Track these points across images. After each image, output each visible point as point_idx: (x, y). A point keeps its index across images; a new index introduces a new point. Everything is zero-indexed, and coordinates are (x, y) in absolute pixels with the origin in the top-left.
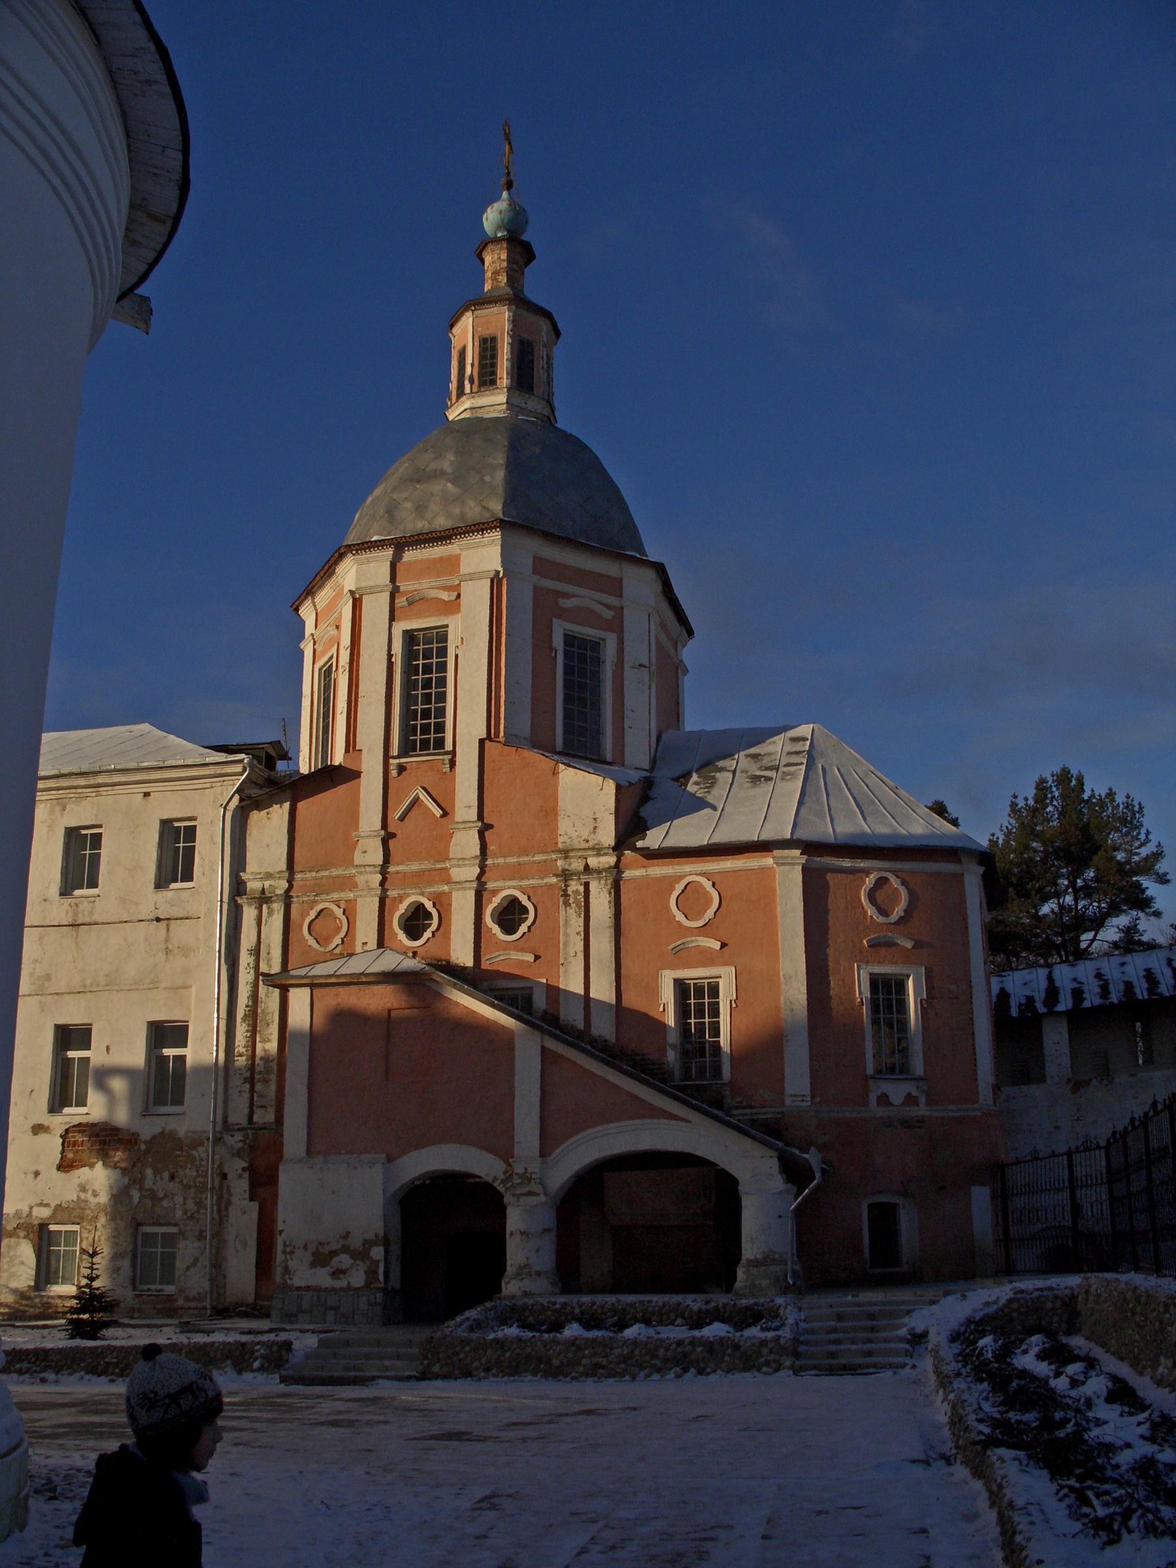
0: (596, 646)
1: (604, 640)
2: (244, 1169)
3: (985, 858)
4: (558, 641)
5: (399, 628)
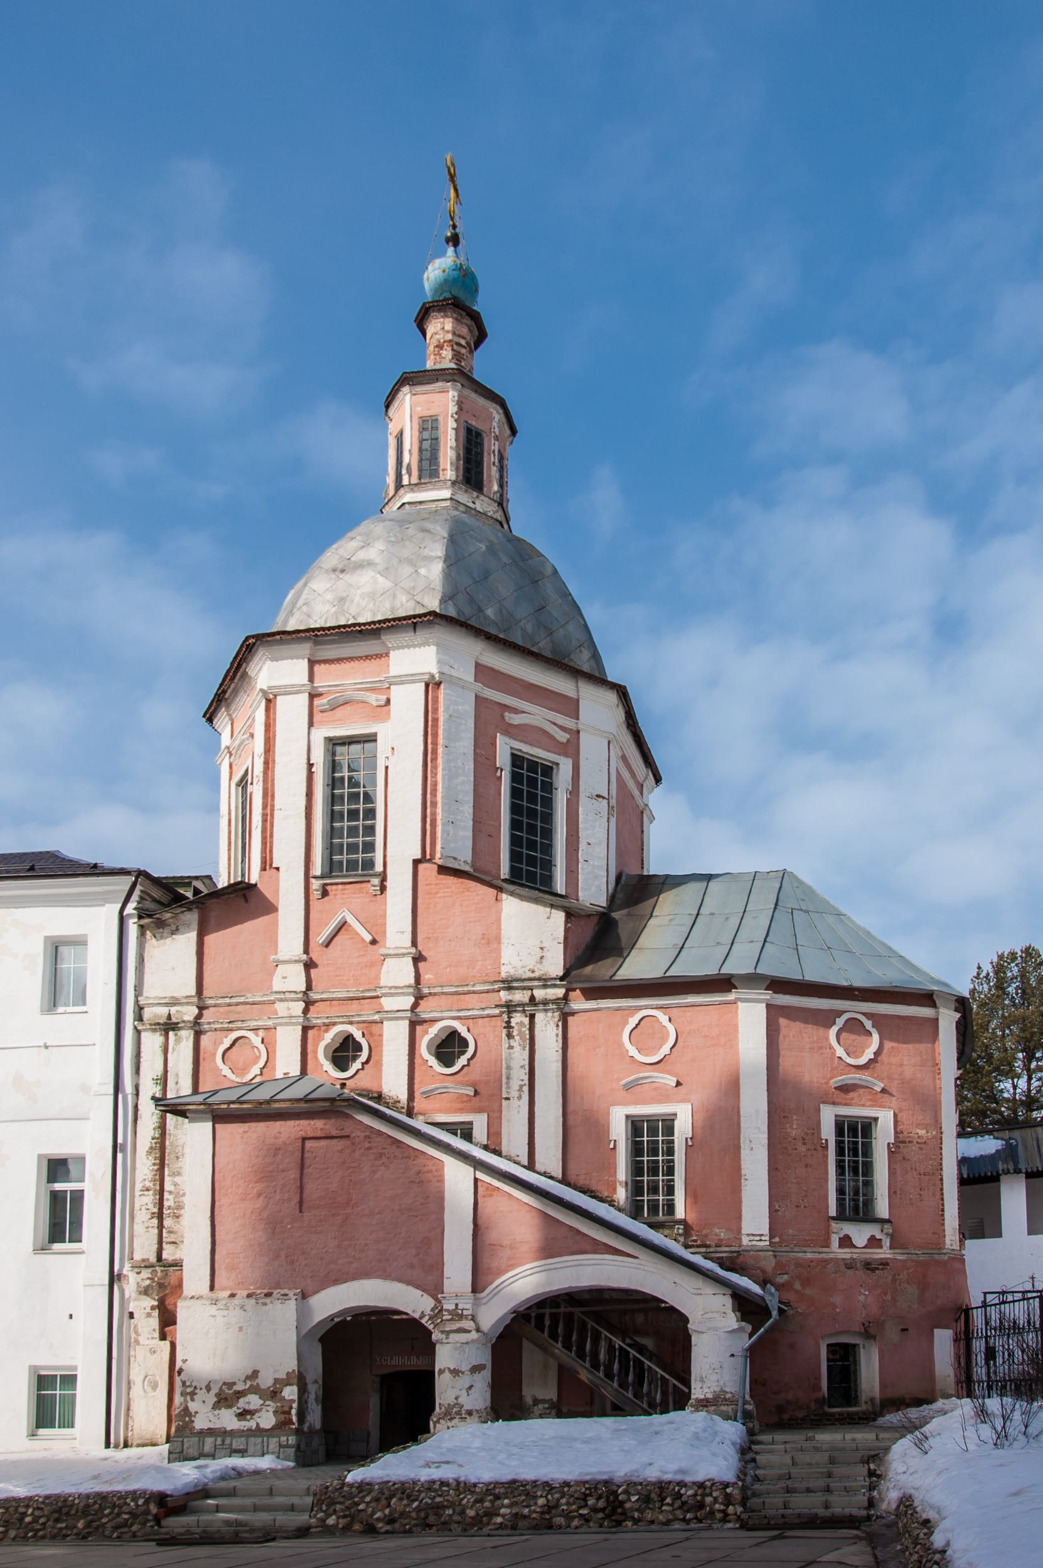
0: (548, 770)
1: (557, 764)
2: (153, 1308)
3: (962, 1004)
4: (503, 759)
5: (320, 735)
